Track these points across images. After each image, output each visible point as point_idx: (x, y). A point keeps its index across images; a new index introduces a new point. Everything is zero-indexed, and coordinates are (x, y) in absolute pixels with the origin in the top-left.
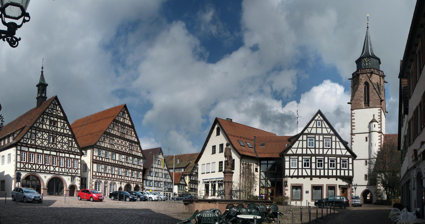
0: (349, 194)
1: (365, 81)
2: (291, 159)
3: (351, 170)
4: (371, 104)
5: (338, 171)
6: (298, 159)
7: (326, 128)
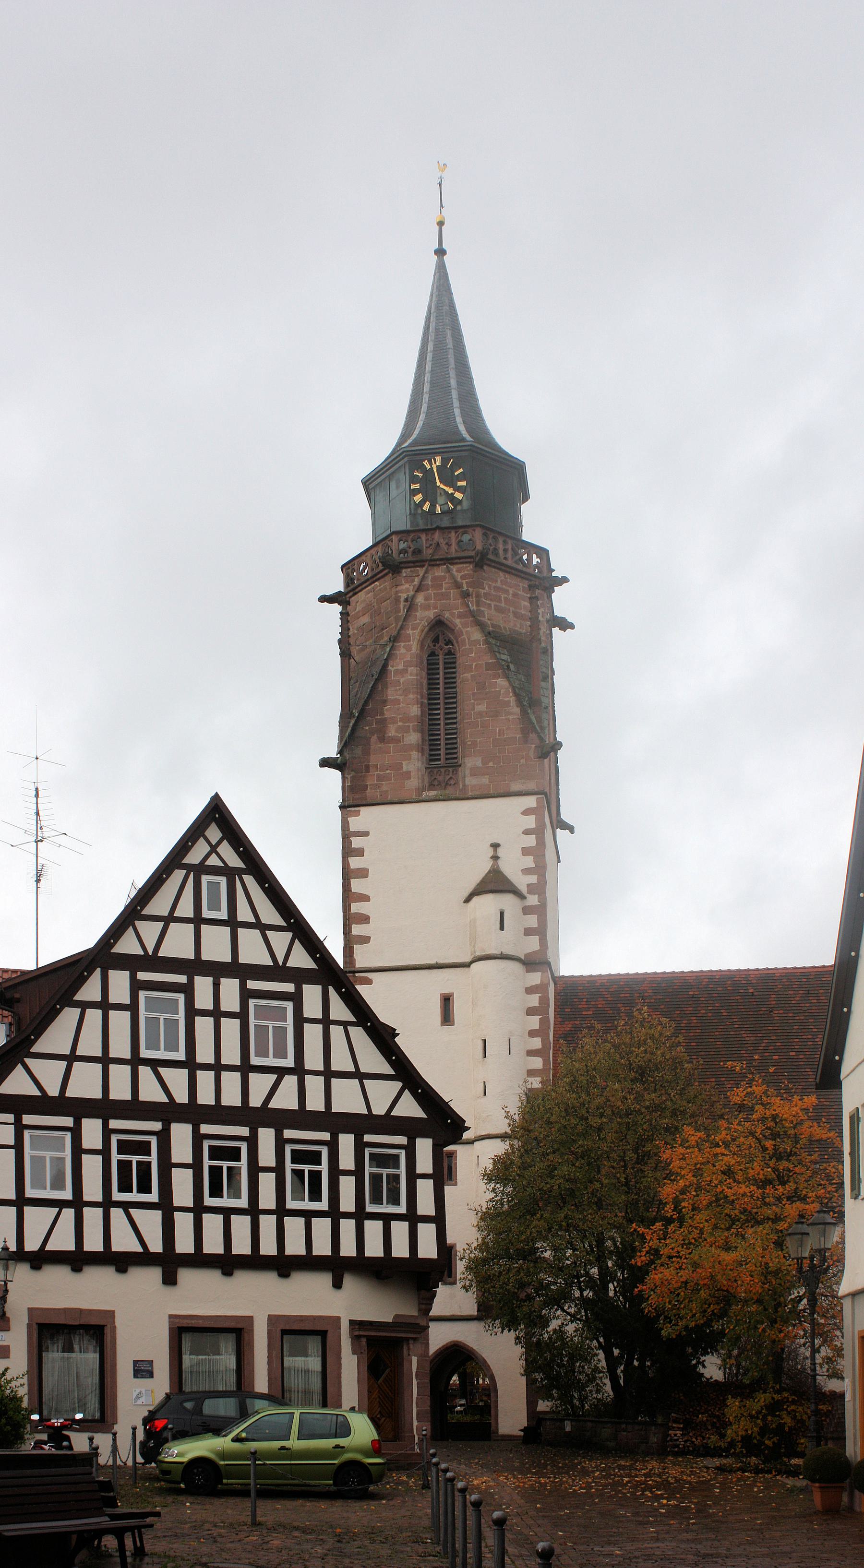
0: (415, 1382)
1: (431, 614)
2: (27, 1134)
3: (426, 1219)
4: (473, 774)
5: (348, 1227)
6: (76, 1132)
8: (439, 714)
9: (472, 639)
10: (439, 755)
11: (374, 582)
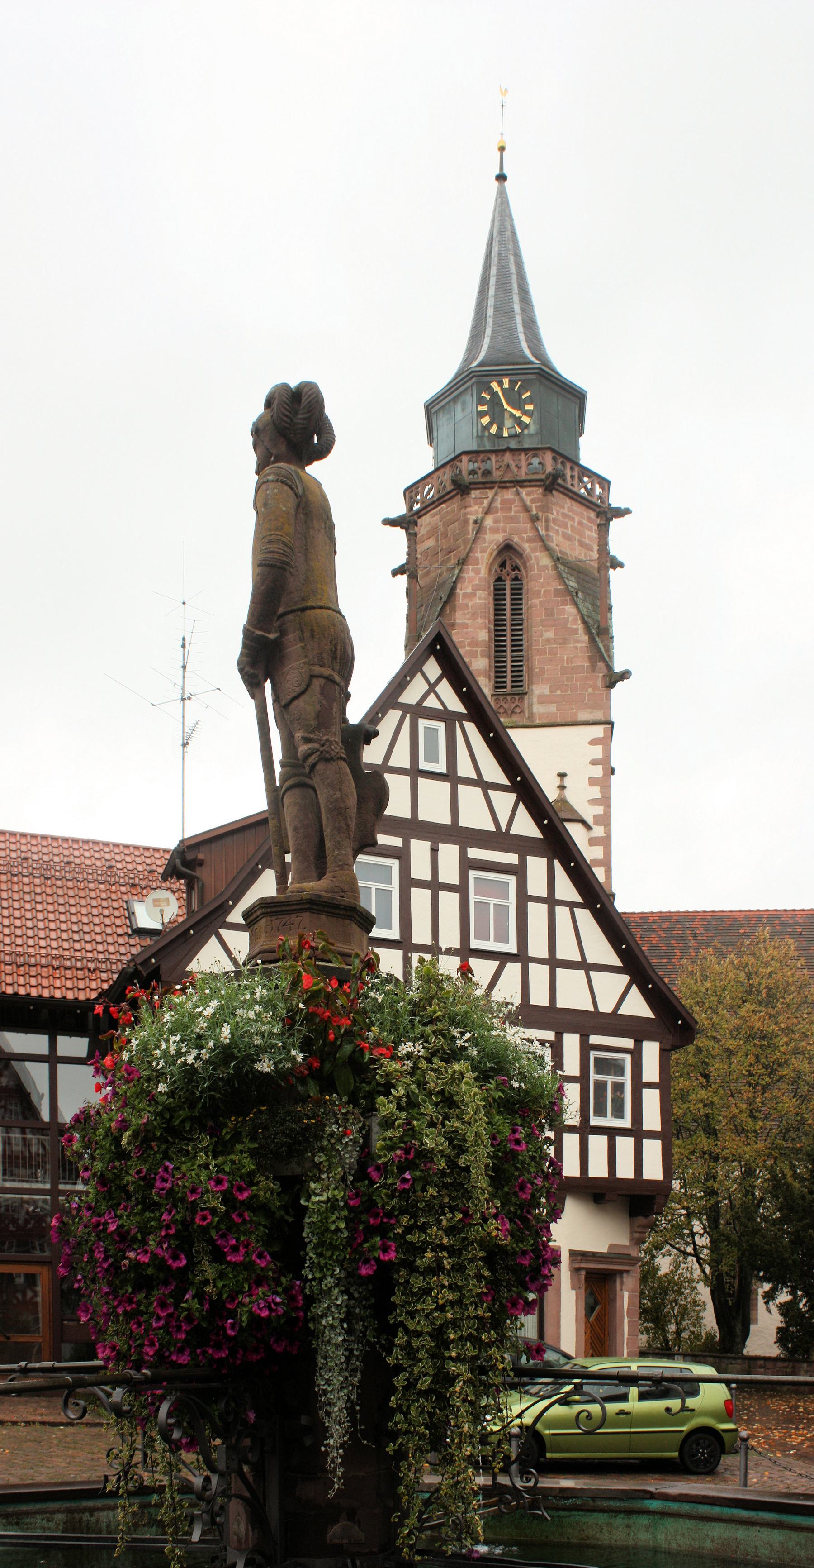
0: (626, 1320)
1: (500, 538)
7: (486, 786)
8: (505, 641)
9: (541, 564)
10: (505, 682)
11: (440, 504)
